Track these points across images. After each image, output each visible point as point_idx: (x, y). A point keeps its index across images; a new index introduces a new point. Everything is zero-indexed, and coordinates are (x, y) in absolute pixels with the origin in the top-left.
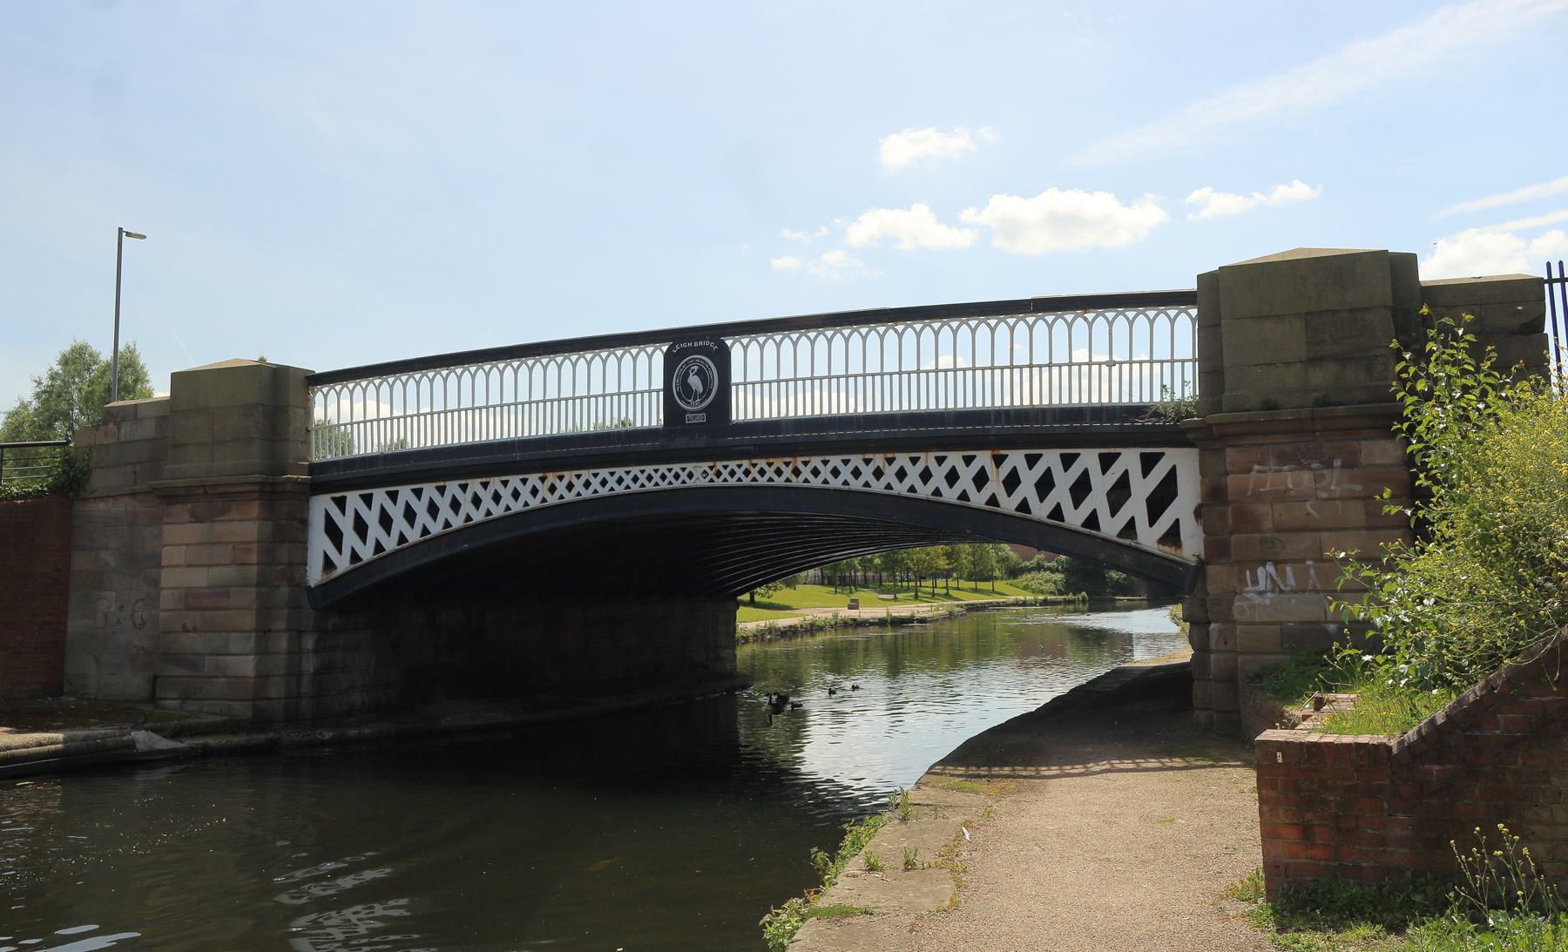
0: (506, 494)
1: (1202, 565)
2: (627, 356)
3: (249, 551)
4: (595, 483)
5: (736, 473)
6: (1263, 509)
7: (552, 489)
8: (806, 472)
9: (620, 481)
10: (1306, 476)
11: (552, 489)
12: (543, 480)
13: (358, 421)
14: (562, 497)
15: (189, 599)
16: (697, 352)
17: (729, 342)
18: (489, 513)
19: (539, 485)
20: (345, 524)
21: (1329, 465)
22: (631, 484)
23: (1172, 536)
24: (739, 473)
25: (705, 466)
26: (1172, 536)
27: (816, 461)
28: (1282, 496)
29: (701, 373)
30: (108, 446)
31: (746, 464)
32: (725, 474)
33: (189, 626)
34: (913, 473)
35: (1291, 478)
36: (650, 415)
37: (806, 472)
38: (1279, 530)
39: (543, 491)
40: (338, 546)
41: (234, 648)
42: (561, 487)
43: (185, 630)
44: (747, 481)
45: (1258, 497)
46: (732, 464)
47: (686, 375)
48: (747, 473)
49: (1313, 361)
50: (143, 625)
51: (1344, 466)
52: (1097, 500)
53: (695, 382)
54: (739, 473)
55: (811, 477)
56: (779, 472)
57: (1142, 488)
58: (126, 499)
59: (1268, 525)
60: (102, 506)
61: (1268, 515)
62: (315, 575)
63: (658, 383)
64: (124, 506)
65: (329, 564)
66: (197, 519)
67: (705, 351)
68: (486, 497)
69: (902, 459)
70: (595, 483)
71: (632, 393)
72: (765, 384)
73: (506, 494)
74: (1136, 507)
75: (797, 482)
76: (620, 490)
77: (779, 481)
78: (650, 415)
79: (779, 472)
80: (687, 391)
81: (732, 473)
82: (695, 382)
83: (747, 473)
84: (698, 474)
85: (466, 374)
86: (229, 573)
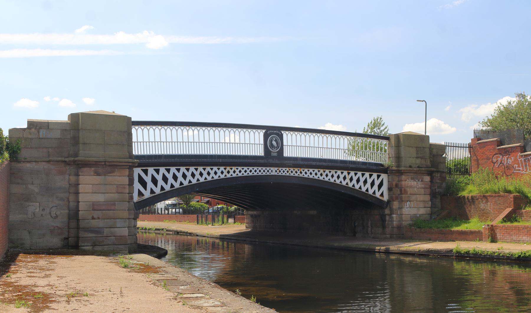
0: (212, 173)
1: (389, 202)
2: (252, 132)
3: (124, 188)
4: (237, 172)
5: (285, 172)
6: (408, 189)
7: (228, 172)
8: (303, 173)
9: (246, 171)
10: (415, 183)
11: (228, 172)
12: (225, 169)
13: (144, 143)
14: (232, 175)
15: (95, 206)
16: (273, 134)
17: (283, 132)
18: (213, 178)
19: (224, 170)
20: (148, 179)
21: (419, 181)
22: (244, 173)
23: (382, 195)
24: (286, 172)
25: (276, 169)
26: (382, 195)
27: (306, 170)
28: (411, 187)
29: (276, 141)
30: (31, 139)
31: (288, 169)
32: (282, 172)
33: (95, 216)
34: (330, 175)
35: (413, 183)
36: (259, 151)
37: (303, 173)
38: (410, 194)
39: (225, 172)
40: (145, 188)
41: (118, 225)
42: (231, 172)
43: (93, 218)
44: (288, 174)
45: (407, 187)
46: (284, 169)
47: (272, 141)
48: (288, 172)
49: (417, 158)
50: (57, 217)
51: (422, 181)
52: (361, 183)
53: (274, 143)
54: (286, 172)
55: (305, 174)
56: (296, 172)
57: (377, 183)
58: (44, 163)
59: (409, 193)
60: (28, 165)
61: (409, 191)
62: (136, 198)
63: (262, 142)
64: (42, 166)
65: (140, 194)
66: (98, 174)
67: (277, 134)
68: (197, 174)
69: (327, 171)
70: (237, 172)
71: (253, 145)
72: (294, 146)
73: (212, 173)
74: (376, 187)
75: (301, 175)
76: (245, 174)
77: (296, 175)
78: (259, 151)
79: (296, 172)
80: (272, 145)
81: (284, 172)
82: (274, 143)
83: (288, 172)
84: (273, 171)
85: (217, 130)
86: (116, 196)
